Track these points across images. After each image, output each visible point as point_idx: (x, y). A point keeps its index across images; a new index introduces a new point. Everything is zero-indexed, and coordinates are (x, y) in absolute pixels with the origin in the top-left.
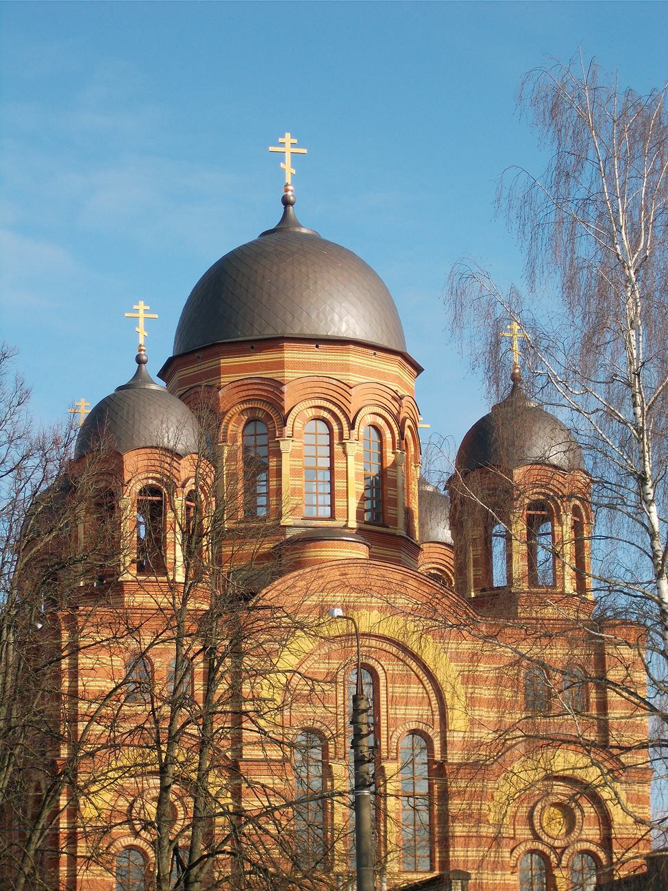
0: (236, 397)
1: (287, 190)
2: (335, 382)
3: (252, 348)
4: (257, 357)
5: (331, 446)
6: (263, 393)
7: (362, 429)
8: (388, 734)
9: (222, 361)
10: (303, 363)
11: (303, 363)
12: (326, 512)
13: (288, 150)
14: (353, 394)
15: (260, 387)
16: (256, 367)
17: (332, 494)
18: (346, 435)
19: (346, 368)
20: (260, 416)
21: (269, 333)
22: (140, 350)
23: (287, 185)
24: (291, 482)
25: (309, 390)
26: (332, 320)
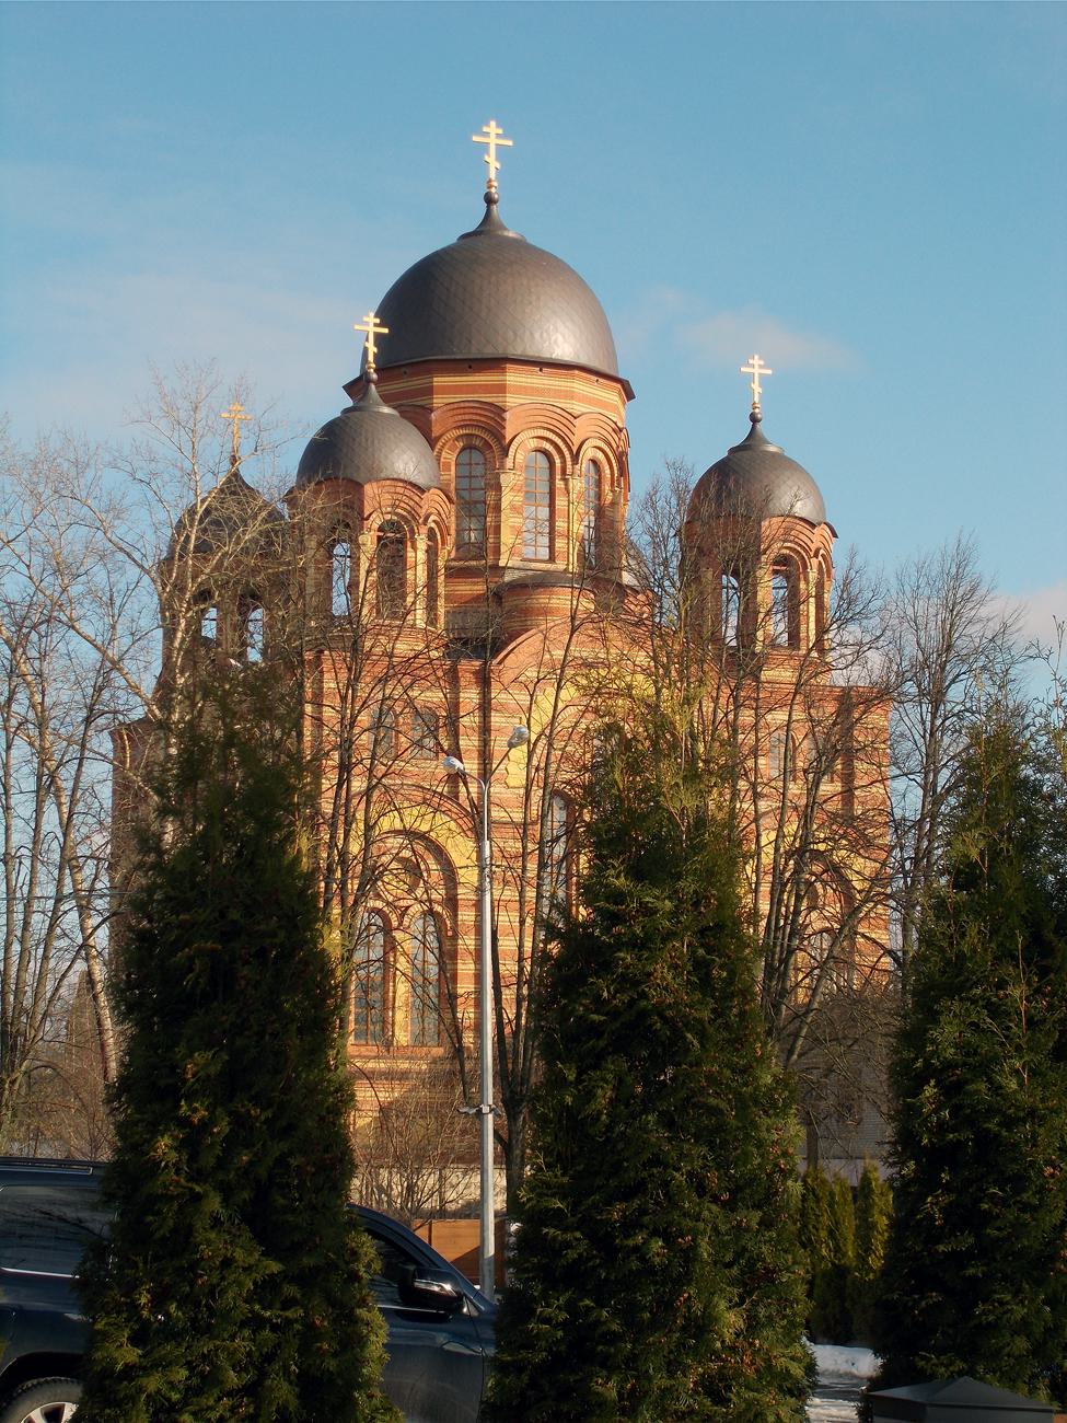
0: (451, 420)
2: (559, 411)
3: (470, 367)
4: (476, 378)
6: (483, 419)
7: (584, 464)
9: (435, 379)
11: (525, 387)
12: (544, 553)
13: (493, 141)
15: (479, 411)
18: (569, 471)
19: (570, 395)
21: (489, 352)
25: (531, 419)
26: (556, 341)
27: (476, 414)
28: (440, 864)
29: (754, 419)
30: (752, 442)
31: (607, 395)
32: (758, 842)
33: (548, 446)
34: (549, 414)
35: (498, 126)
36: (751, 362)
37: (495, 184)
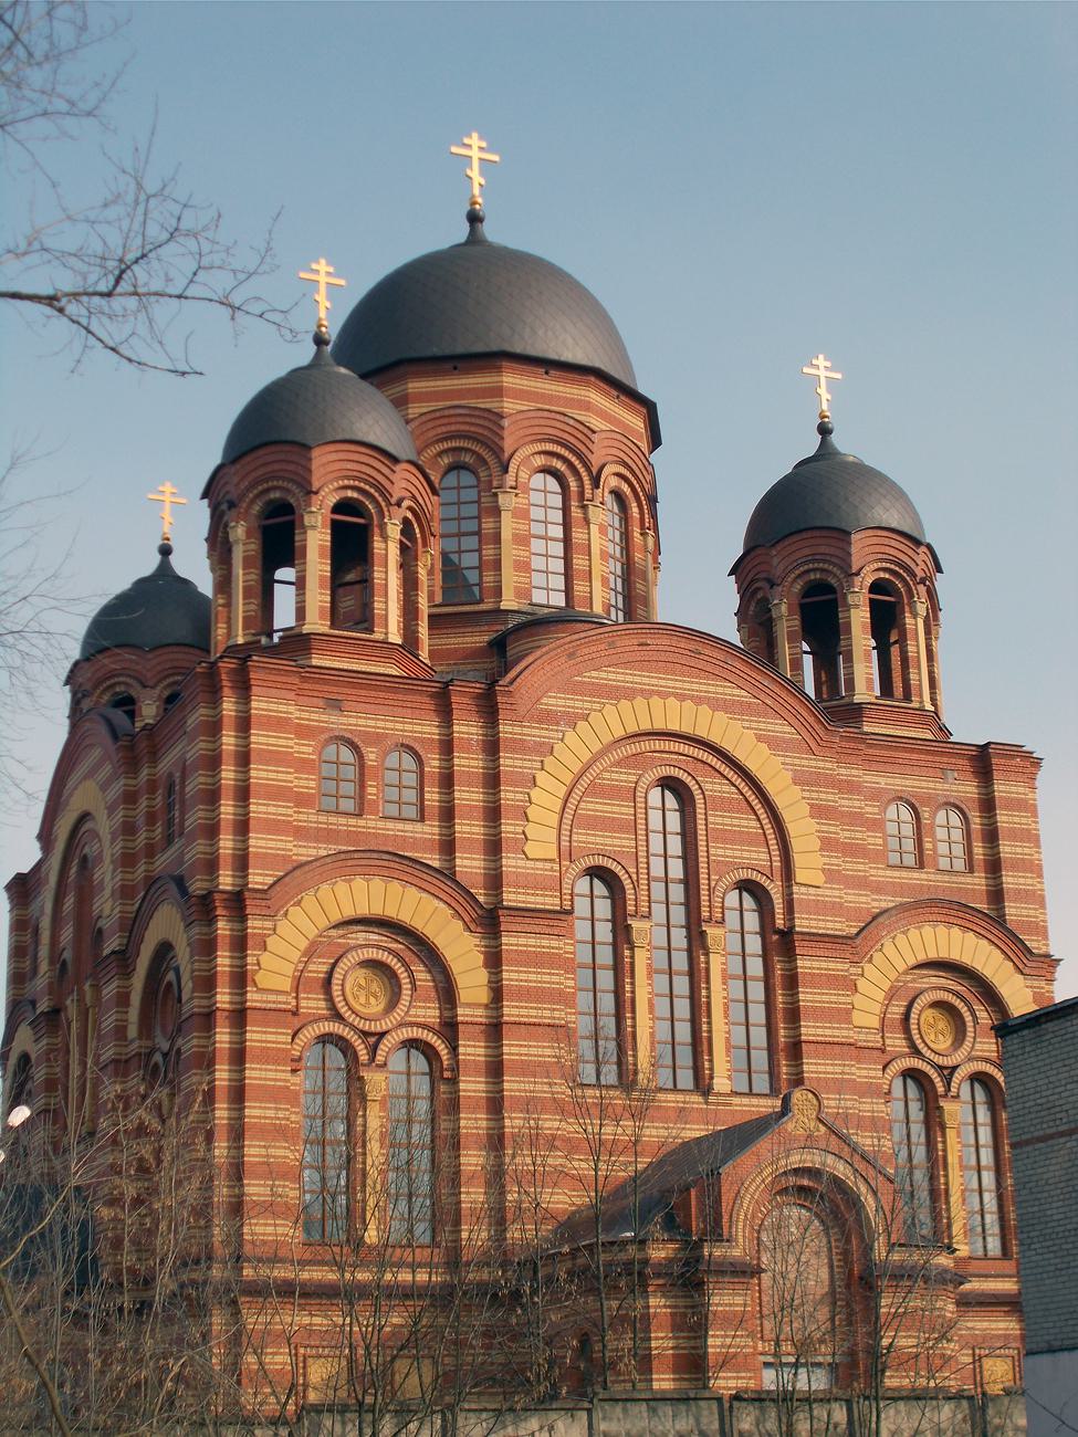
1: (320, 326)
2: (571, 422)
4: (471, 381)
5: (566, 510)
9: (410, 385)
15: (468, 420)
16: (460, 394)
18: (588, 495)
23: (320, 319)
24: (515, 552)
28: (430, 972)
29: (824, 430)
30: (825, 451)
33: (559, 465)
34: (558, 425)
35: (481, 138)
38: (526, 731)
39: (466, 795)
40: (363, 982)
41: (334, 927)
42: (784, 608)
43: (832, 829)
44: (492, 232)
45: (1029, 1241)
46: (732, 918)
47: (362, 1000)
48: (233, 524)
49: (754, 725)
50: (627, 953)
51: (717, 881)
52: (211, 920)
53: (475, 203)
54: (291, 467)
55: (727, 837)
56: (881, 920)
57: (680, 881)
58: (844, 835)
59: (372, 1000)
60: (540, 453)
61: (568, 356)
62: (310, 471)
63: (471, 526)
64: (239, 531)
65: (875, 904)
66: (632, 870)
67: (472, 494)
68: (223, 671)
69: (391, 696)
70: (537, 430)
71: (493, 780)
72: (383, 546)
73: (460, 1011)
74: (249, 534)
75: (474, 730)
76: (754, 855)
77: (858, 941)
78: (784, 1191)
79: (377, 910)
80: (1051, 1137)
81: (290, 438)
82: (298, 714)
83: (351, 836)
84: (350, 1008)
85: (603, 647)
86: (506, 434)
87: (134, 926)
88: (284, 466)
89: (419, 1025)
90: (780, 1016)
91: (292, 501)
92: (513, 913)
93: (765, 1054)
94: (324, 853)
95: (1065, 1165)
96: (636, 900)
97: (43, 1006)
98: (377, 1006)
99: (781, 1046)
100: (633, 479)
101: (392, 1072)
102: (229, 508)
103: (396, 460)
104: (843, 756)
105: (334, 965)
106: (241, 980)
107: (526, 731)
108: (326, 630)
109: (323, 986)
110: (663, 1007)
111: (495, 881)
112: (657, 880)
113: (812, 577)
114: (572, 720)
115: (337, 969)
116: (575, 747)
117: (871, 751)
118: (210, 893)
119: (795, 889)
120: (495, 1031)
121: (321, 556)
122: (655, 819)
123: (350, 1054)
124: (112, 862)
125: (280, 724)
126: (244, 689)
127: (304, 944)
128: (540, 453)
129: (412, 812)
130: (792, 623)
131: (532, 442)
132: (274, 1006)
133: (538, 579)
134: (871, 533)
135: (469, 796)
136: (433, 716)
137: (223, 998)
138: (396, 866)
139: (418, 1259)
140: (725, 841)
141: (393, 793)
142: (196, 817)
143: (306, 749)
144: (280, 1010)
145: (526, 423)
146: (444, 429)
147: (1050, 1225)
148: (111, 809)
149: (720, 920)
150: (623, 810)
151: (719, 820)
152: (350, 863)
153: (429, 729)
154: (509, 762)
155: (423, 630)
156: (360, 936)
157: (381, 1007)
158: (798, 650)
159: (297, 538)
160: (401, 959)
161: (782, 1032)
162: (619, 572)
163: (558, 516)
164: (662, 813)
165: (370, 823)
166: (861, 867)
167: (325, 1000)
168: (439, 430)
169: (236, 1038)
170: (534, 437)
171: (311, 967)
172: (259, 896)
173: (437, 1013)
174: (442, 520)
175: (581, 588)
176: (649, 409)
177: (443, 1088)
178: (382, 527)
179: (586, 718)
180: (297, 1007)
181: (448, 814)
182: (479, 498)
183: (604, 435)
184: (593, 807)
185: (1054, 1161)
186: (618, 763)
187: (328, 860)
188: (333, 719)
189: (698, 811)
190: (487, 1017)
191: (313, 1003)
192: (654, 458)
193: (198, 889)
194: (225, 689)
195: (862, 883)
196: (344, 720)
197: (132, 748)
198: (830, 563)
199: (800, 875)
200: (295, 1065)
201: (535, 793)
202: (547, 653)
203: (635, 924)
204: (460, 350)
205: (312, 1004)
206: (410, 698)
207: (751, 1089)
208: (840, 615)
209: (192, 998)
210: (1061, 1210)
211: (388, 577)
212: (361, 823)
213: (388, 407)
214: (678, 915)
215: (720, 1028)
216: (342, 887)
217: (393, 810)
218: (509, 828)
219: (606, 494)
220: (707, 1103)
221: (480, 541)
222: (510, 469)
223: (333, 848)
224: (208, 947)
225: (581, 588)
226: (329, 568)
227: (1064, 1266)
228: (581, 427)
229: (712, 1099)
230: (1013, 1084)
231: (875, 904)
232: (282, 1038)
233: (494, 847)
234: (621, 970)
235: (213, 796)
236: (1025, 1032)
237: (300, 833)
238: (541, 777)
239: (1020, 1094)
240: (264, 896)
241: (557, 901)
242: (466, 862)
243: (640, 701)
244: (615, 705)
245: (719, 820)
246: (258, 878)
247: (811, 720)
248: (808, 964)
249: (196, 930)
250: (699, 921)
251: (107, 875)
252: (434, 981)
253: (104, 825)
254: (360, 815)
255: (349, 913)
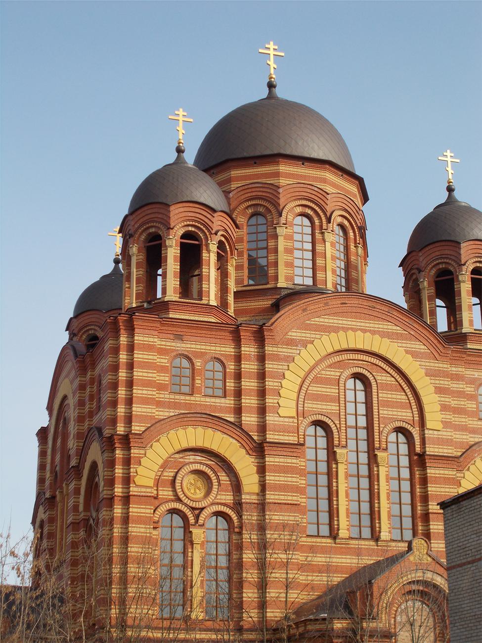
2: (316, 189)
5: (313, 235)
8: (379, 430)
9: (232, 173)
10: (293, 174)
14: (329, 199)
15: (261, 189)
17: (314, 268)
18: (324, 227)
20: (261, 210)
22: (179, 143)
24: (285, 257)
27: (263, 192)
28: (228, 476)
29: (450, 190)
30: (451, 200)
31: (351, 187)
32: (425, 603)
33: (309, 212)
36: (445, 154)
37: (274, 76)
38: (280, 350)
39: (248, 384)
40: (193, 482)
41: (178, 453)
42: (426, 284)
43: (447, 400)
44: (281, 93)
45: (455, 622)
46: (392, 448)
47: (192, 491)
48: (131, 246)
49: (404, 345)
50: (334, 466)
51: (384, 428)
52: (113, 450)
53: (272, 78)
54: (160, 216)
55: (388, 404)
56: (474, 448)
57: (364, 428)
58: (454, 403)
59: (198, 491)
60: (299, 206)
61: (314, 155)
62: (170, 217)
63: (262, 244)
64: (134, 249)
65: (472, 439)
66: (337, 422)
67: (263, 228)
68: (120, 321)
69: (209, 332)
70: (297, 194)
71: (262, 376)
72: (208, 255)
73: (243, 497)
74: (139, 251)
75: (252, 350)
76: (404, 414)
77: (461, 459)
78: (409, 592)
79: (200, 444)
80: (464, 564)
81: (160, 201)
82: (159, 343)
83: (187, 405)
84: (185, 495)
85: (321, 305)
86: (281, 196)
87: (82, 453)
88: (156, 215)
89: (222, 504)
90: (418, 499)
91: (160, 233)
92: (271, 445)
93: (410, 520)
94: (173, 414)
95: (470, 580)
96: (339, 438)
97: (48, 495)
98: (200, 494)
99: (419, 515)
100: (350, 218)
101: (207, 529)
102: (130, 238)
103: (214, 211)
104: (453, 361)
105: (177, 473)
106: (127, 480)
107: (280, 350)
108: (177, 299)
109: (171, 484)
110: (354, 494)
111: (262, 428)
112: (351, 427)
113: (441, 266)
114: (305, 344)
115: (179, 475)
116: (306, 358)
117: (469, 358)
118: (112, 435)
119: (426, 432)
120: (262, 506)
121: (175, 261)
122: (350, 395)
123: (186, 519)
124: (74, 420)
125: (150, 348)
126: (131, 330)
127: (160, 462)
128: (299, 206)
129: (220, 393)
130: (430, 291)
131: (295, 200)
132: (144, 494)
133: (298, 271)
134: (472, 242)
135: (249, 384)
136: (253, 343)
137: (118, 490)
138: (210, 421)
139: (164, 626)
140: (388, 406)
141: (210, 383)
142: (106, 397)
143: (164, 361)
144: (288, 504)
145: (292, 190)
146: (249, 195)
147: (463, 613)
148: (74, 393)
149: (385, 448)
150: (332, 391)
151: (385, 395)
152: (186, 419)
153: (229, 349)
154: (270, 366)
155: (231, 299)
156: (191, 458)
157: (202, 494)
158: (434, 305)
159: (163, 252)
160: (212, 469)
161: (419, 508)
162: (343, 267)
163: (309, 238)
164: (354, 392)
165: (197, 399)
166: (463, 420)
167: (172, 491)
168: (247, 195)
169: (125, 511)
170: (296, 197)
171: (165, 474)
172: (137, 437)
173: (232, 498)
174: (248, 242)
175: (321, 275)
176: (360, 182)
177: (234, 537)
178: (207, 245)
179: (312, 342)
180: (157, 494)
181: (238, 394)
182: (267, 229)
183: (334, 195)
184: (315, 389)
185: (466, 577)
186: (330, 366)
187: (174, 418)
188: (178, 345)
189: (373, 391)
190: (258, 500)
191: (166, 493)
192: (365, 209)
193: (107, 434)
194: (122, 331)
195: (464, 428)
196: (184, 345)
197: (84, 362)
198: (450, 259)
199: (429, 424)
200: (155, 525)
201: (284, 382)
202: (291, 309)
203: (338, 451)
204: (258, 153)
205: (165, 493)
206: (219, 333)
207: (402, 539)
208: (455, 286)
209: (103, 490)
210: (468, 605)
211: (211, 270)
212: (192, 398)
213: (215, 187)
214: (363, 446)
215: (384, 505)
216: (181, 432)
217: (210, 392)
218: (270, 400)
219: (334, 226)
220: (377, 546)
221: (267, 252)
222: (283, 214)
223: (177, 412)
224: (111, 464)
225: (321, 275)
226: (179, 267)
227: (469, 636)
228: (321, 192)
229: (380, 543)
230: (448, 535)
231: (472, 439)
232: (148, 511)
233: (262, 411)
234: (331, 475)
235: (115, 386)
236: (453, 506)
237: (159, 404)
238: (287, 374)
239: (451, 540)
240: (140, 437)
241: (296, 439)
242: (248, 419)
243: (341, 334)
244: (328, 336)
245: (385, 395)
246: (137, 428)
247: (436, 342)
248: (433, 471)
249: (106, 455)
250: (374, 449)
251: (72, 428)
252: (230, 481)
253: (72, 401)
254: (192, 395)
255: (185, 445)
